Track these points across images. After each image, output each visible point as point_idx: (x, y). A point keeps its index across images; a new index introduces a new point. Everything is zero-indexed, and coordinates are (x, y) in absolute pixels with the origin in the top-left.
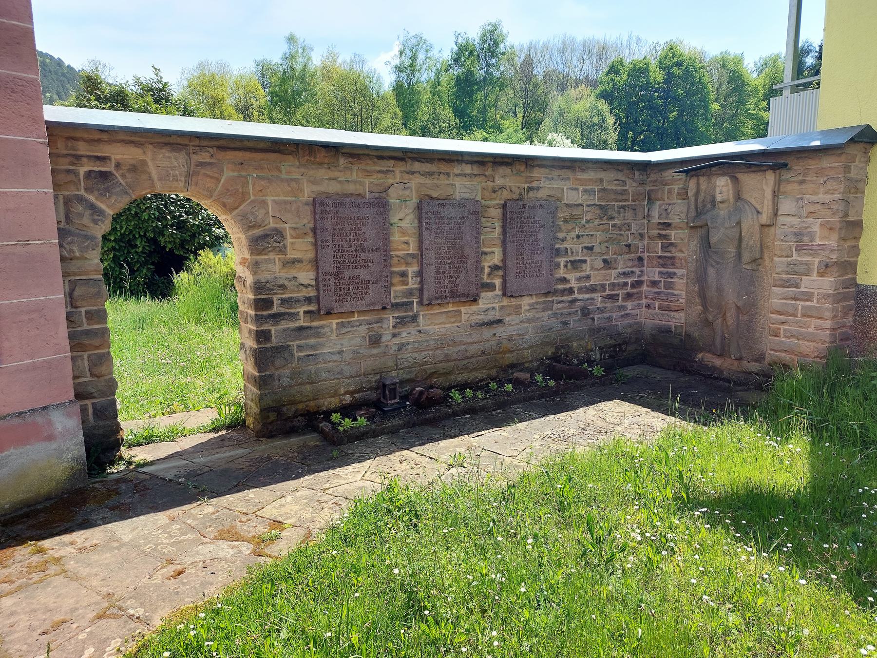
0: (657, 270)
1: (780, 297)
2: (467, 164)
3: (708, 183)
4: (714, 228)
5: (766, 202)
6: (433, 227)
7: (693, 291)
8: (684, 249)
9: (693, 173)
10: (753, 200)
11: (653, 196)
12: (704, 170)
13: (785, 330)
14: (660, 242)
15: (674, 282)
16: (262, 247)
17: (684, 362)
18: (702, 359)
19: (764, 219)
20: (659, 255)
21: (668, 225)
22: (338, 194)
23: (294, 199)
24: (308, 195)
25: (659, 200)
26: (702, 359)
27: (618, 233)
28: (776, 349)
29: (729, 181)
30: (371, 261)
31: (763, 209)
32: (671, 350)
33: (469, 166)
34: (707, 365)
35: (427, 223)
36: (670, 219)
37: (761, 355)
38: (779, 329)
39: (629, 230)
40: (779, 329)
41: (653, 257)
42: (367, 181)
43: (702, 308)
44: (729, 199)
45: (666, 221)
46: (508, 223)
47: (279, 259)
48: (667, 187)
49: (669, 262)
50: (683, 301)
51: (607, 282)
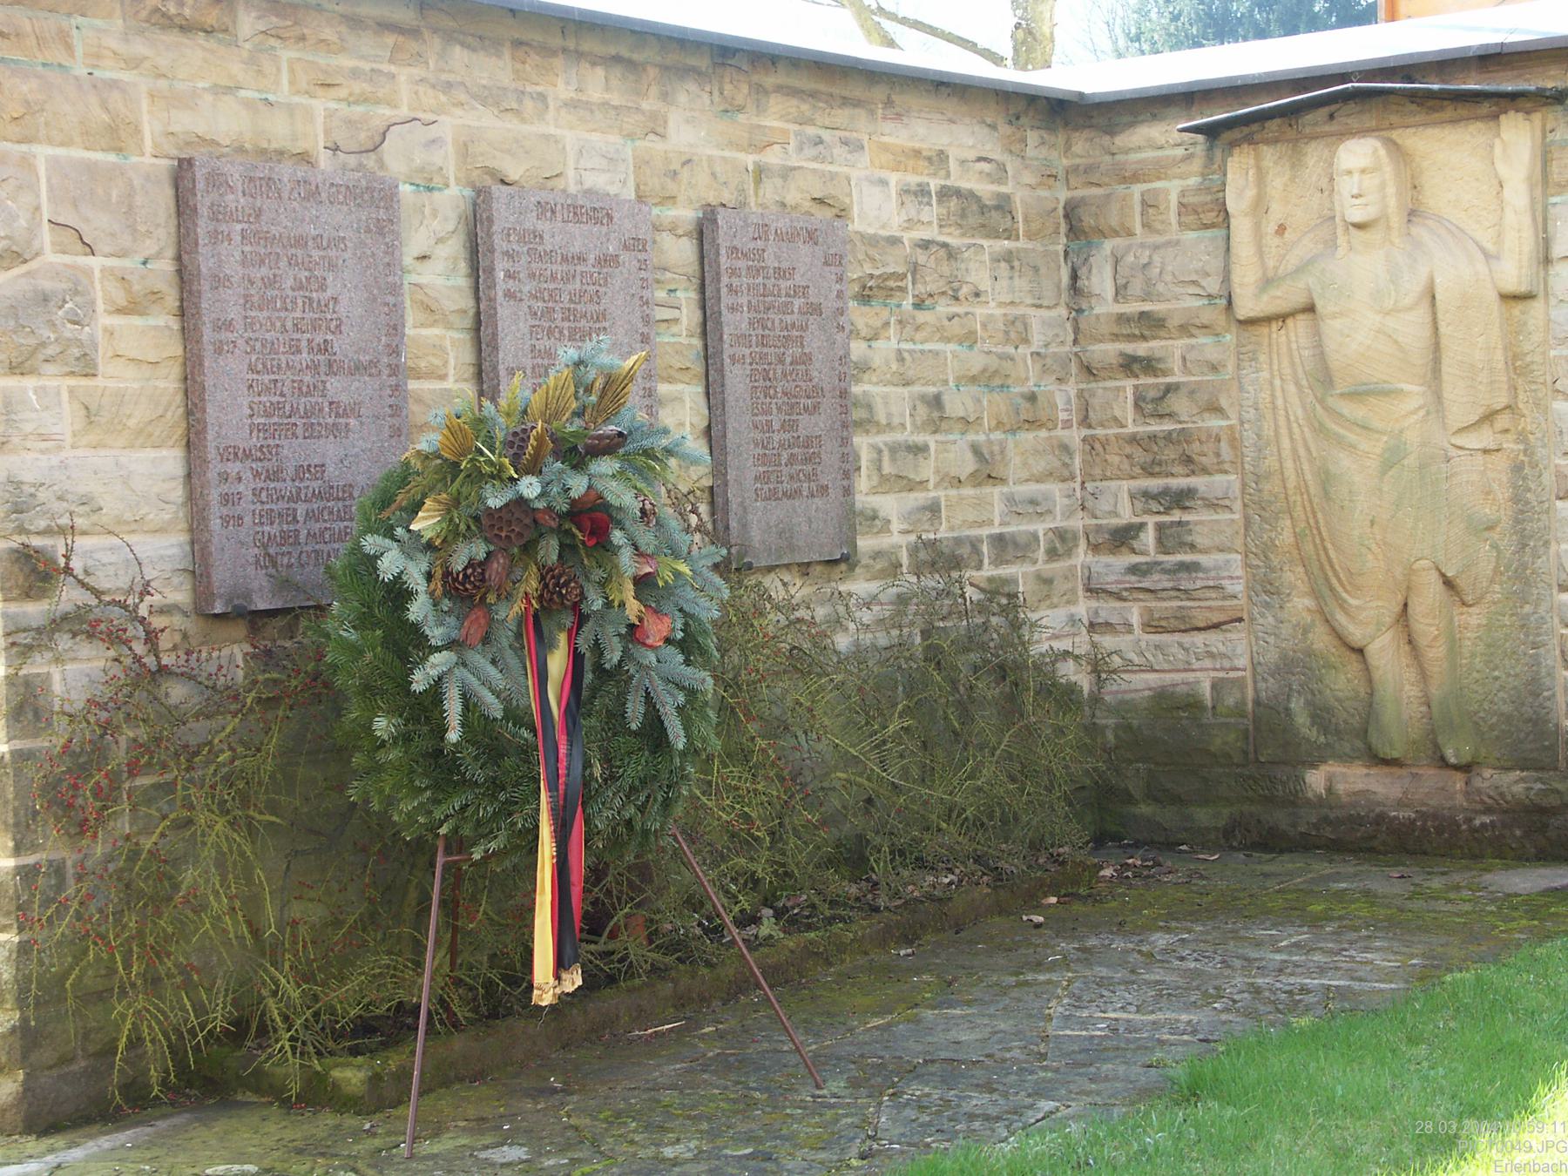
0: (1126, 485)
2: (594, 64)
5: (1510, 217)
6: (526, 289)
9: (1236, 134)
11: (1088, 221)
12: (1273, 125)
14: (1129, 384)
16: (32, 341)
19: (1513, 274)
20: (1131, 429)
21: (1151, 324)
22: (241, 150)
23: (112, 157)
24: (156, 145)
25: (1116, 234)
27: (999, 349)
29: (1382, 152)
30: (353, 410)
31: (1499, 238)
33: (600, 72)
35: (510, 275)
36: (1160, 298)
39: (1026, 341)
41: (1105, 444)
42: (321, 105)
45: (1147, 307)
46: (724, 291)
47: (71, 391)
48: (1137, 189)
49: (1170, 453)
50: (1238, 587)
51: (985, 532)
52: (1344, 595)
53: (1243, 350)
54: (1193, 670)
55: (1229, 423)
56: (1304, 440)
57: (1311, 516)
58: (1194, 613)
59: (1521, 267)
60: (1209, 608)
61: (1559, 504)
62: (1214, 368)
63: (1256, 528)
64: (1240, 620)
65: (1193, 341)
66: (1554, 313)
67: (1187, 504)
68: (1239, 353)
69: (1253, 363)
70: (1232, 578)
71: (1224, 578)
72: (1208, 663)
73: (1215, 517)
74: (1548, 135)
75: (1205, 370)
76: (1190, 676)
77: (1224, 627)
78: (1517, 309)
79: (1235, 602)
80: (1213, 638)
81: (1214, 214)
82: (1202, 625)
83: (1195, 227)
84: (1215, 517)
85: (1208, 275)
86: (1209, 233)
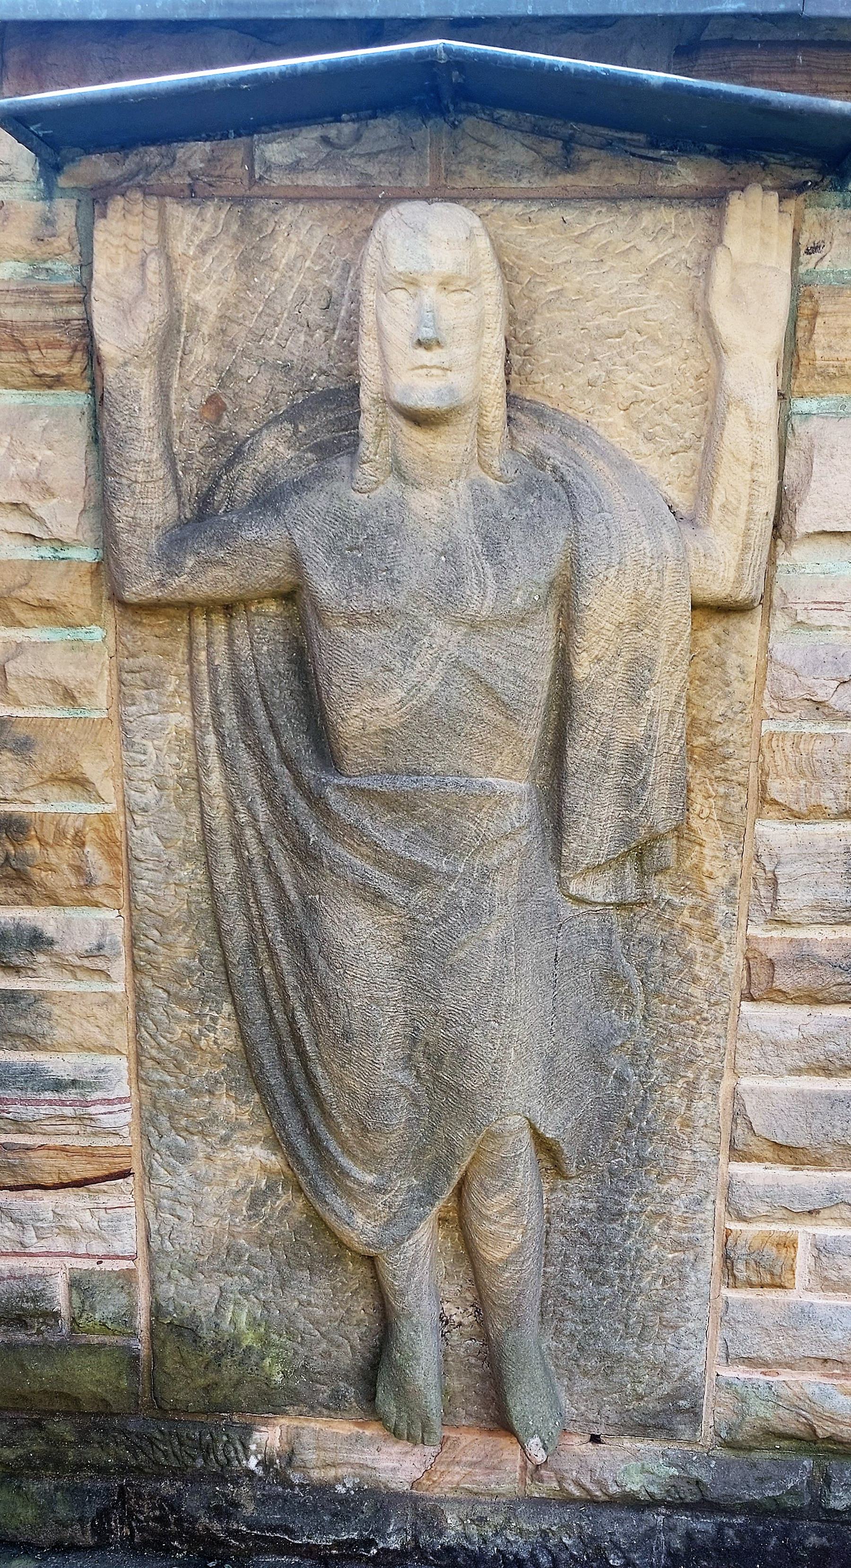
1: (793, 1059)
3: (245, 263)
4: (374, 619)
7: (193, 1046)
8: (92, 768)
10: (617, 418)
13: (821, 1250)
15: (40, 997)
17: (165, 1487)
18: (290, 1457)
26: (290, 1457)
28: (767, 1354)
32: (62, 1428)
34: (323, 1489)
37: (673, 1397)
38: (788, 1244)
40: (788, 1244)
43: (275, 1161)
44: (479, 403)
52: (344, 1161)
53: (130, 663)
54: (32, 1255)
55: (99, 808)
56: (268, 862)
57: (289, 1047)
58: (36, 1158)
59: (746, 548)
60: (63, 1149)
61: (746, 1007)
62: (68, 696)
63: (158, 1013)
64: (125, 1174)
65: (17, 634)
66: (779, 649)
67: (16, 961)
68: (120, 669)
69: (153, 693)
70: (109, 1102)
71: (95, 1103)
72: (61, 1244)
73: (73, 987)
74: (804, 258)
75: (48, 697)
76: (29, 1265)
77: (92, 1187)
78: (716, 627)
79: (115, 1141)
80: (69, 1199)
81: (62, 354)
82: (49, 1180)
83: (16, 380)
84: (73, 987)
85: (48, 492)
86: (47, 399)
